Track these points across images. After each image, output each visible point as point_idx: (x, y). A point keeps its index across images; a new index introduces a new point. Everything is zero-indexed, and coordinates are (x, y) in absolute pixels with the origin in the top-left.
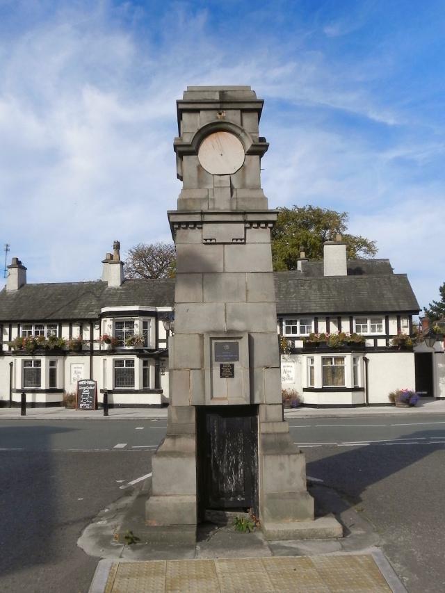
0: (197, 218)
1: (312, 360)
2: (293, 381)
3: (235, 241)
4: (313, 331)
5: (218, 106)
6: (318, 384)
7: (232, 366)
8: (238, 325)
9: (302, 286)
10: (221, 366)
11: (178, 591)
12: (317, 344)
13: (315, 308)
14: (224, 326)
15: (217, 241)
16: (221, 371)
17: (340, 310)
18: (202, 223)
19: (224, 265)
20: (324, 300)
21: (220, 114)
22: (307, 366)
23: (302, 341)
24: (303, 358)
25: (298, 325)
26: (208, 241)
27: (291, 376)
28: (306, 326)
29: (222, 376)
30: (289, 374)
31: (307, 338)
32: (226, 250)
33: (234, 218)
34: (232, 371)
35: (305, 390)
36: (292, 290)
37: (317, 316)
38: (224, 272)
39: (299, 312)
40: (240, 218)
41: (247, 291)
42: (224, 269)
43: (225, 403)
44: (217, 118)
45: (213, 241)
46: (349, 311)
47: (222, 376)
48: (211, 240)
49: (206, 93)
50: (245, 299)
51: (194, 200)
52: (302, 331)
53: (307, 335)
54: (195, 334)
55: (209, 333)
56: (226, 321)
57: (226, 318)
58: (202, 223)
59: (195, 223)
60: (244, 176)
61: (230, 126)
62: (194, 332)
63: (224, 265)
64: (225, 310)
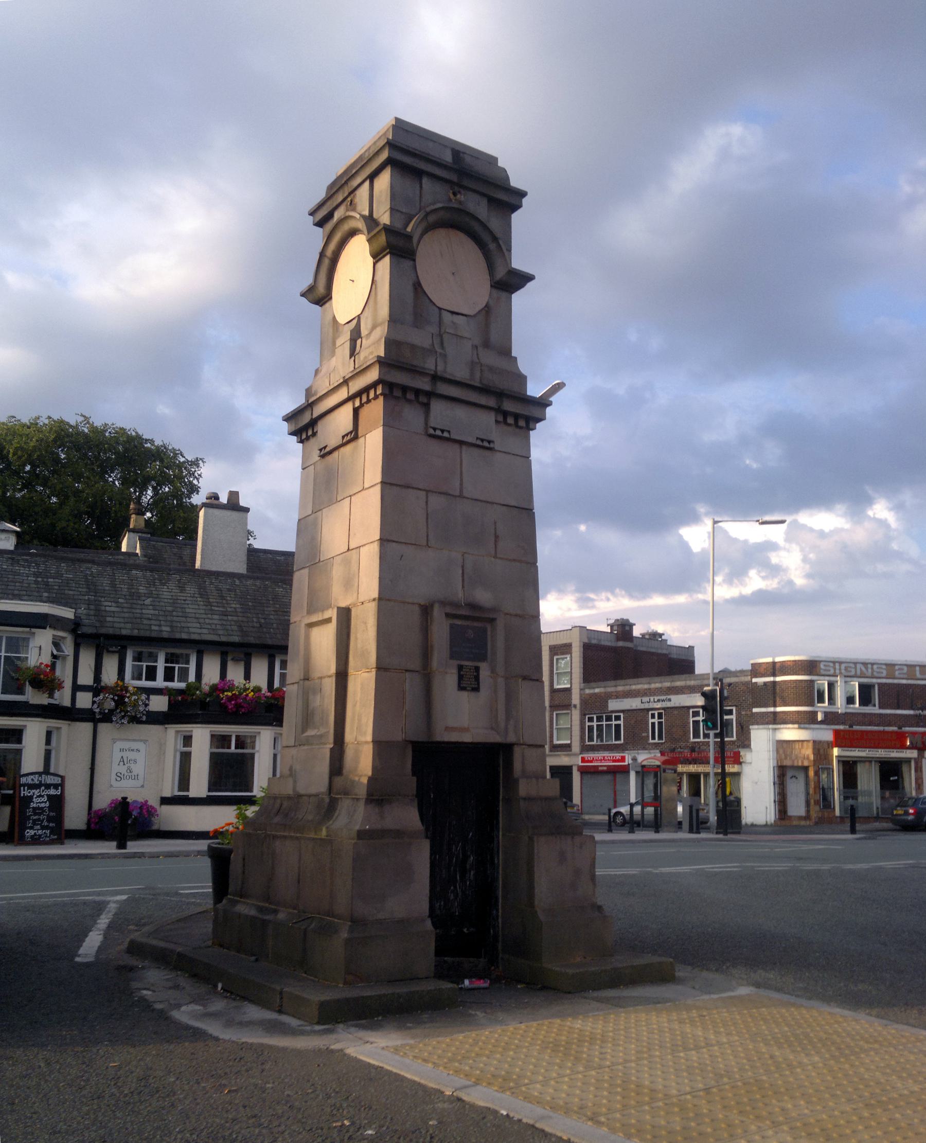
0: (424, 384)
1: (188, 740)
2: (140, 783)
3: (479, 442)
4: (192, 678)
5: (454, 177)
6: (199, 786)
7: (477, 669)
8: (483, 597)
9: (164, 584)
10: (460, 668)
11: (430, 1065)
12: (203, 704)
13: (196, 631)
14: (460, 595)
15: (454, 436)
16: (461, 678)
17: (252, 640)
18: (430, 394)
19: (461, 484)
20: (215, 617)
21: (455, 194)
22: (176, 751)
23: (166, 698)
24: (171, 734)
25: (161, 665)
26: (438, 433)
27: (135, 773)
28: (177, 666)
29: (461, 688)
30: (132, 766)
31: (180, 692)
32: (464, 455)
33: (483, 400)
34: (477, 678)
35: (165, 801)
36: (142, 590)
37: (202, 647)
38: (461, 496)
39: (165, 635)
40: (492, 402)
41: (496, 537)
42: (461, 491)
43: (467, 738)
44: (450, 200)
45: (446, 435)
46: (270, 642)
47: (461, 688)
48: (443, 431)
49: (431, 144)
50: (493, 552)
51: (413, 347)
52: (169, 676)
53: (177, 685)
54: (413, 604)
55: (443, 603)
56: (463, 587)
57: (463, 580)
58: (430, 394)
59: (417, 392)
60: (487, 325)
61: (474, 224)
62: (410, 600)
63: (461, 484)
64: (463, 567)
